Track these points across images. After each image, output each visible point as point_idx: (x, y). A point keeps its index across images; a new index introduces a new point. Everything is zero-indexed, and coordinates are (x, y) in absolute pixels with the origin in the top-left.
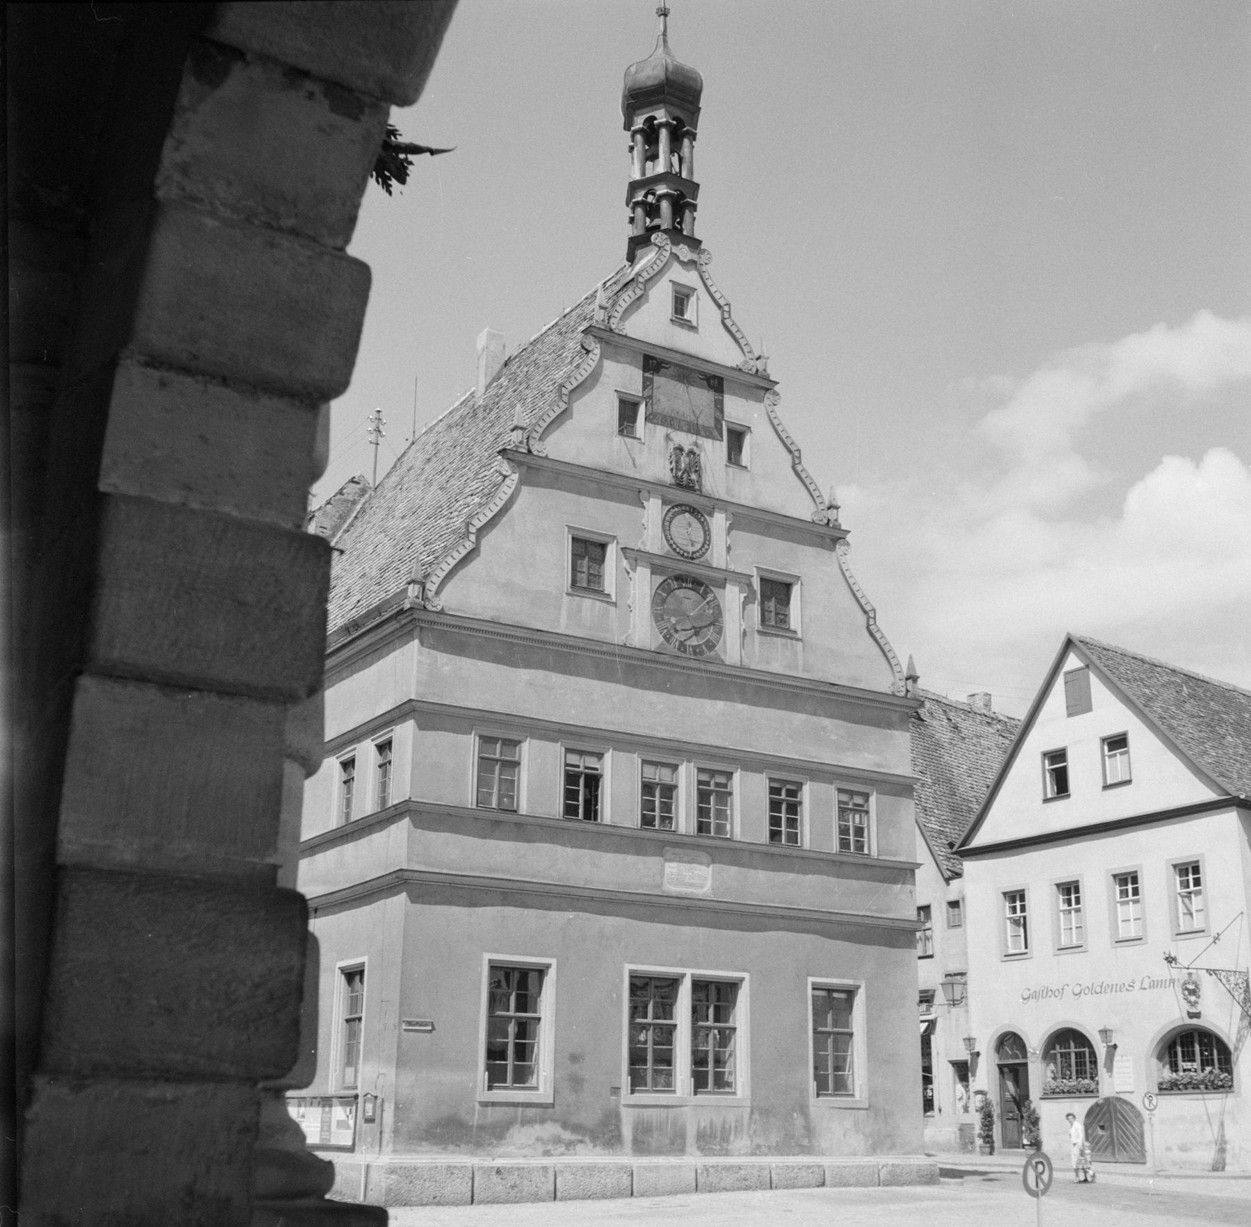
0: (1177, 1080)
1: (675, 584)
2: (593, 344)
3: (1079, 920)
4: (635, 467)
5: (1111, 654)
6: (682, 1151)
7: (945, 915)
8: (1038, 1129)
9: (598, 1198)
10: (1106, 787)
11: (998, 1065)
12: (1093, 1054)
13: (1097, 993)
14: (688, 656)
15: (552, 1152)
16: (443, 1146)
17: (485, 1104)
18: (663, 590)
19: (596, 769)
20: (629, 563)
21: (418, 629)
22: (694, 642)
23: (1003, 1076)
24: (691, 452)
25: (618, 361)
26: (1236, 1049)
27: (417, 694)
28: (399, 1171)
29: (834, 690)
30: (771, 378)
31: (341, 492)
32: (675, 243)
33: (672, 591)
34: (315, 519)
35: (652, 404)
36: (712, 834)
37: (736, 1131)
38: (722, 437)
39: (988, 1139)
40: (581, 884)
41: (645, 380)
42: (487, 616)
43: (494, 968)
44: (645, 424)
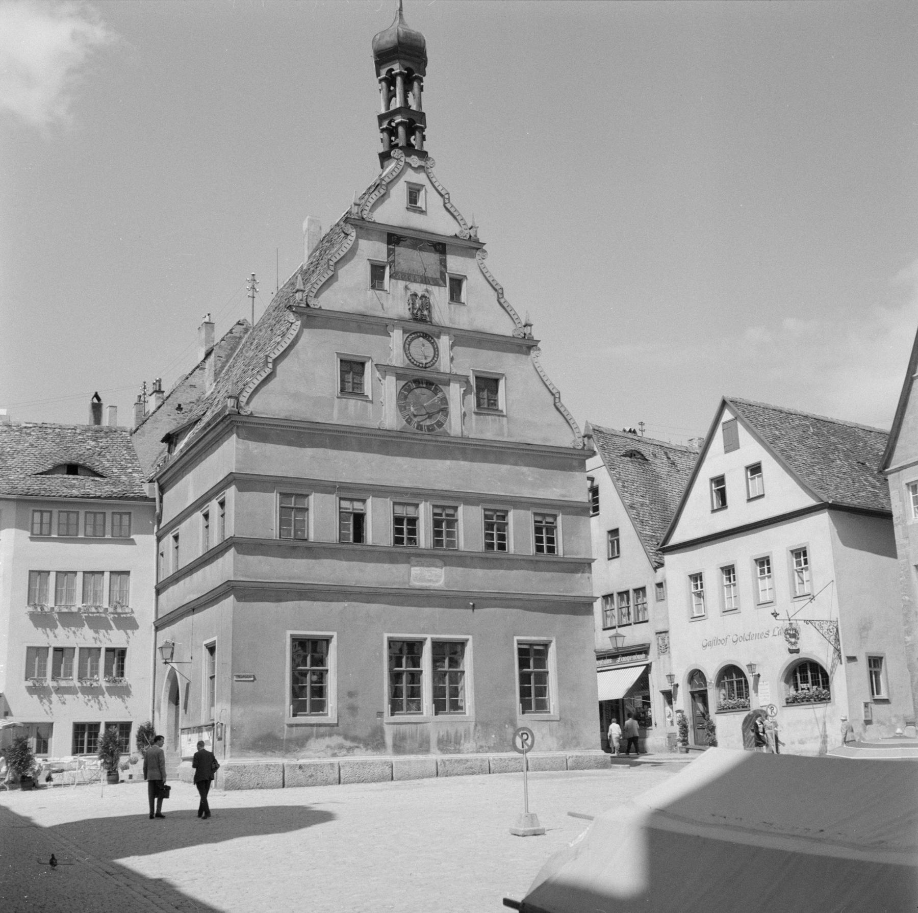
0: (797, 696)
1: (414, 386)
2: (351, 230)
3: (735, 591)
4: (384, 310)
5: (754, 409)
6: (427, 751)
7: (654, 592)
8: (715, 734)
9: (369, 782)
10: (749, 500)
11: (690, 692)
12: (746, 681)
13: (747, 640)
14: (423, 432)
15: (338, 754)
16: (264, 753)
17: (291, 726)
18: (405, 390)
19: (362, 510)
20: (381, 374)
21: (235, 428)
22: (428, 422)
23: (694, 700)
24: (423, 296)
25: (369, 239)
26: (831, 672)
27: (236, 469)
28: (233, 768)
29: (528, 447)
30: (480, 241)
31: (231, 332)
32: (408, 155)
33: (412, 390)
34: (214, 351)
35: (394, 266)
36: (444, 547)
37: (465, 737)
38: (445, 283)
39: (685, 742)
40: (353, 584)
41: (389, 250)
42: (282, 416)
43: (392, 642)
44: (390, 280)
